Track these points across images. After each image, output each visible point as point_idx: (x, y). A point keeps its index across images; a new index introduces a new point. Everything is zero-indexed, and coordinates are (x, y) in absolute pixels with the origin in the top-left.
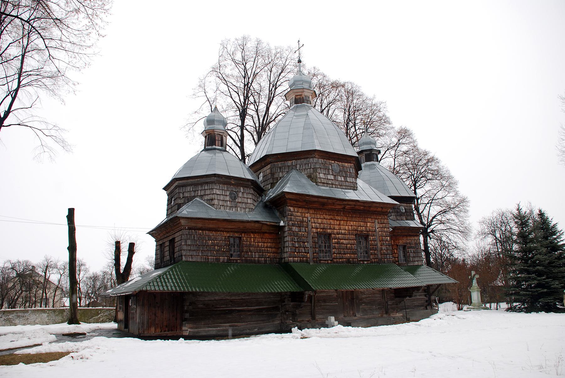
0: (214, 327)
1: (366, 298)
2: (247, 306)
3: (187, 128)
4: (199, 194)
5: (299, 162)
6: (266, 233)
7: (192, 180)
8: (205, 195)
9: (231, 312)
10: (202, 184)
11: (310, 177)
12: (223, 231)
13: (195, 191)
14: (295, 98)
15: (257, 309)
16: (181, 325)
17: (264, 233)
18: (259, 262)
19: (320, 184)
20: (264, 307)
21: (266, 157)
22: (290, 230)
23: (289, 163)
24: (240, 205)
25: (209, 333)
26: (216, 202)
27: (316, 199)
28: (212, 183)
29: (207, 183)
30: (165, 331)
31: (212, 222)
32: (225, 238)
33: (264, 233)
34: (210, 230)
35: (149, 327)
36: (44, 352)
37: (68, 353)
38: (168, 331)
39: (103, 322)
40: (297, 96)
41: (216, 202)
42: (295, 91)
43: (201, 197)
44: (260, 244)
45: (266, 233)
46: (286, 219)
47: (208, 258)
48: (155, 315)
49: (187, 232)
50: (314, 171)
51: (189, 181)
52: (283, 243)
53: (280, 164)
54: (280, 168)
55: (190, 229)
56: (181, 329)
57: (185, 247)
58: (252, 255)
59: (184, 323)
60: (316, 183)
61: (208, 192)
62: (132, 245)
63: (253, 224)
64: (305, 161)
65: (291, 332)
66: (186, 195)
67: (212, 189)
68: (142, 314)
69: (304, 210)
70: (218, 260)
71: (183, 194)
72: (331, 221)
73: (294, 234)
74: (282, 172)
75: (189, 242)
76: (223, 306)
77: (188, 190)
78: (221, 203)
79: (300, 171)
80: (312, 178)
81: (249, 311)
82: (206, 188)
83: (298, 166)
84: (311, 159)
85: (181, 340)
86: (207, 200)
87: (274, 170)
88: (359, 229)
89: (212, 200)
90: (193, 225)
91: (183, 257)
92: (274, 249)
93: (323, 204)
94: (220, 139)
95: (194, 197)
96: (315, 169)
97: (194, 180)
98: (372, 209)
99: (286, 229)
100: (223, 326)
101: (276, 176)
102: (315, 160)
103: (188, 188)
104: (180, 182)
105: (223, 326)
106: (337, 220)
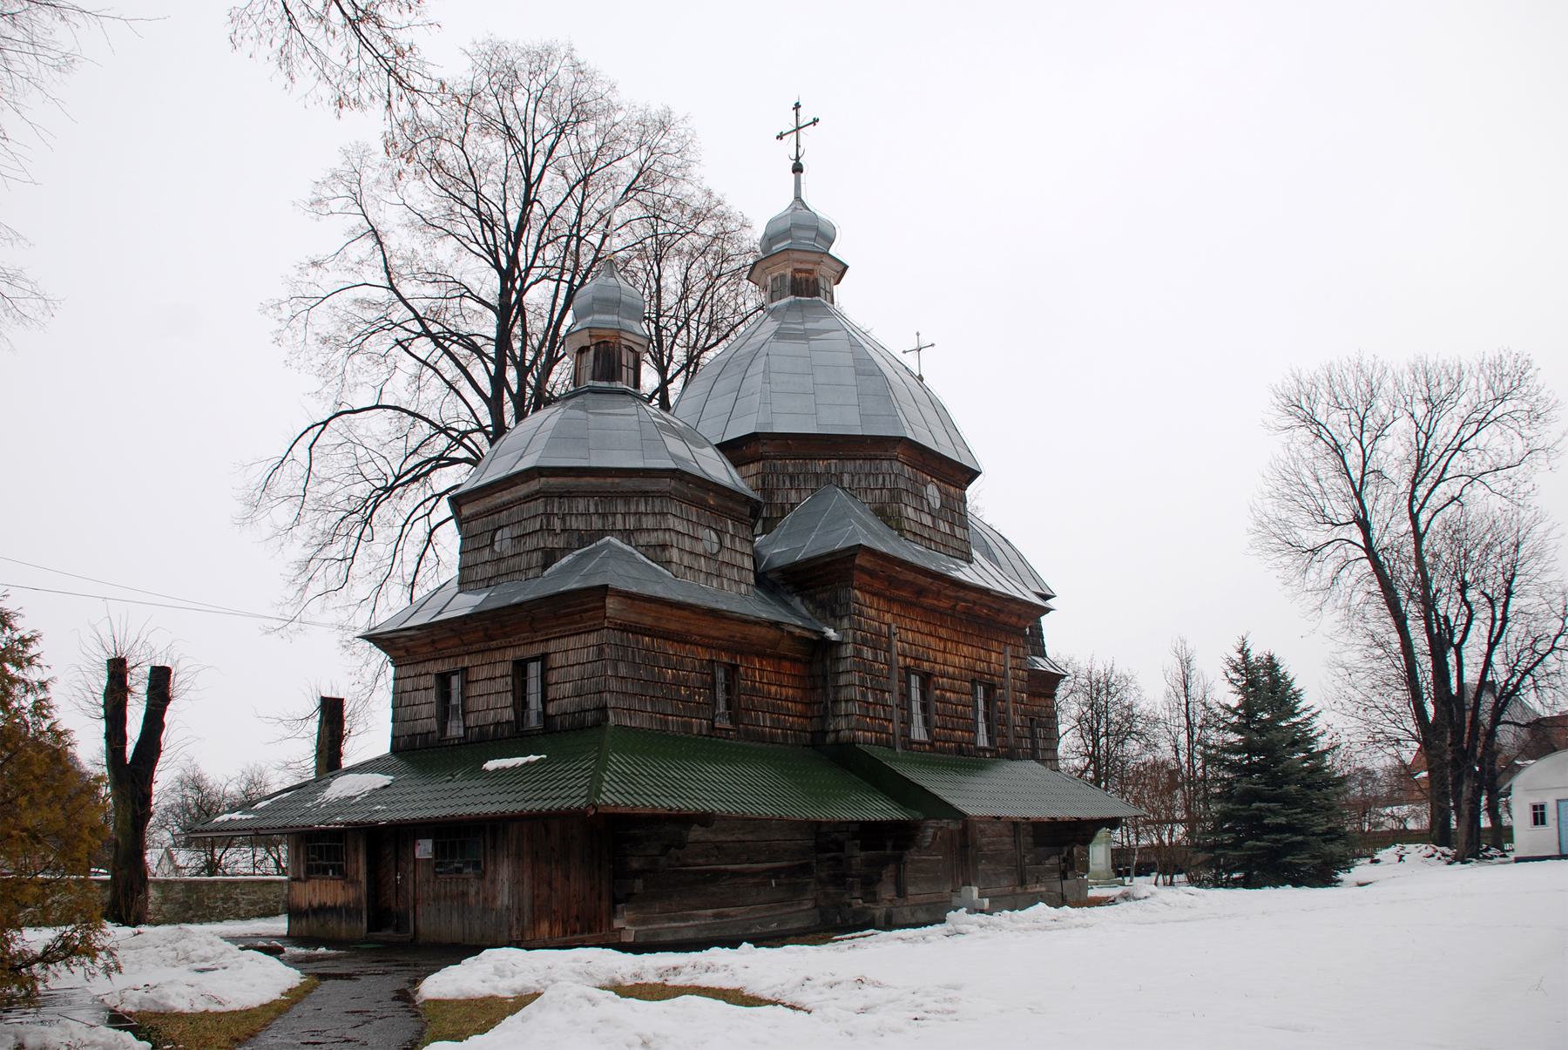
0: (683, 919)
1: (989, 844)
2: (749, 861)
3: (286, 312)
4: (619, 526)
5: (850, 466)
6: (785, 657)
7: (592, 480)
8: (640, 530)
9: (717, 875)
10: (627, 496)
11: (880, 512)
12: (697, 644)
13: (604, 516)
14: (794, 279)
15: (768, 870)
16: (613, 913)
17: (782, 658)
18: (772, 739)
19: (908, 535)
20: (784, 864)
21: (754, 437)
22: (858, 654)
23: (820, 466)
24: (725, 571)
25: (679, 937)
26: (675, 554)
27: (910, 576)
28: (661, 495)
29: (645, 494)
30: (574, 932)
31: (679, 612)
32: (702, 666)
33: (782, 658)
34: (668, 636)
35: (535, 921)
36: (256, 1005)
37: (523, 1000)
38: (582, 932)
39: (247, 917)
40: (800, 271)
41: (675, 554)
42: (796, 255)
43: (627, 535)
44: (773, 689)
45: (785, 657)
46: (846, 623)
47: (666, 722)
48: (550, 884)
49: (616, 637)
50: (892, 497)
51: (584, 481)
52: (831, 691)
53: (790, 466)
54: (792, 478)
55: (625, 628)
56: (610, 924)
57: (614, 684)
58: (757, 718)
59: (619, 906)
60: (901, 531)
61: (648, 522)
62: (160, 680)
63: (764, 630)
64: (867, 466)
65: (943, 921)
66: (576, 523)
67: (663, 514)
68: (517, 882)
69: (883, 605)
70: (687, 727)
71: (563, 520)
72: (931, 639)
73: (864, 667)
74: (798, 490)
75: (623, 671)
76: (701, 861)
77: (581, 508)
78: (687, 560)
79: (852, 492)
80: (887, 516)
81: (755, 874)
82: (642, 508)
83: (846, 478)
84: (885, 464)
85: (746, 946)
86: (648, 546)
87: (773, 481)
88: (980, 666)
89: (664, 547)
90: (633, 617)
91: (610, 713)
92: (800, 706)
93: (921, 592)
94: (631, 365)
95: (602, 533)
96: (895, 495)
97: (601, 481)
98: (1002, 617)
99: (849, 650)
100: (699, 916)
101: (778, 499)
102: (897, 466)
103: (581, 505)
104: (552, 480)
105: (699, 916)
106: (940, 638)
